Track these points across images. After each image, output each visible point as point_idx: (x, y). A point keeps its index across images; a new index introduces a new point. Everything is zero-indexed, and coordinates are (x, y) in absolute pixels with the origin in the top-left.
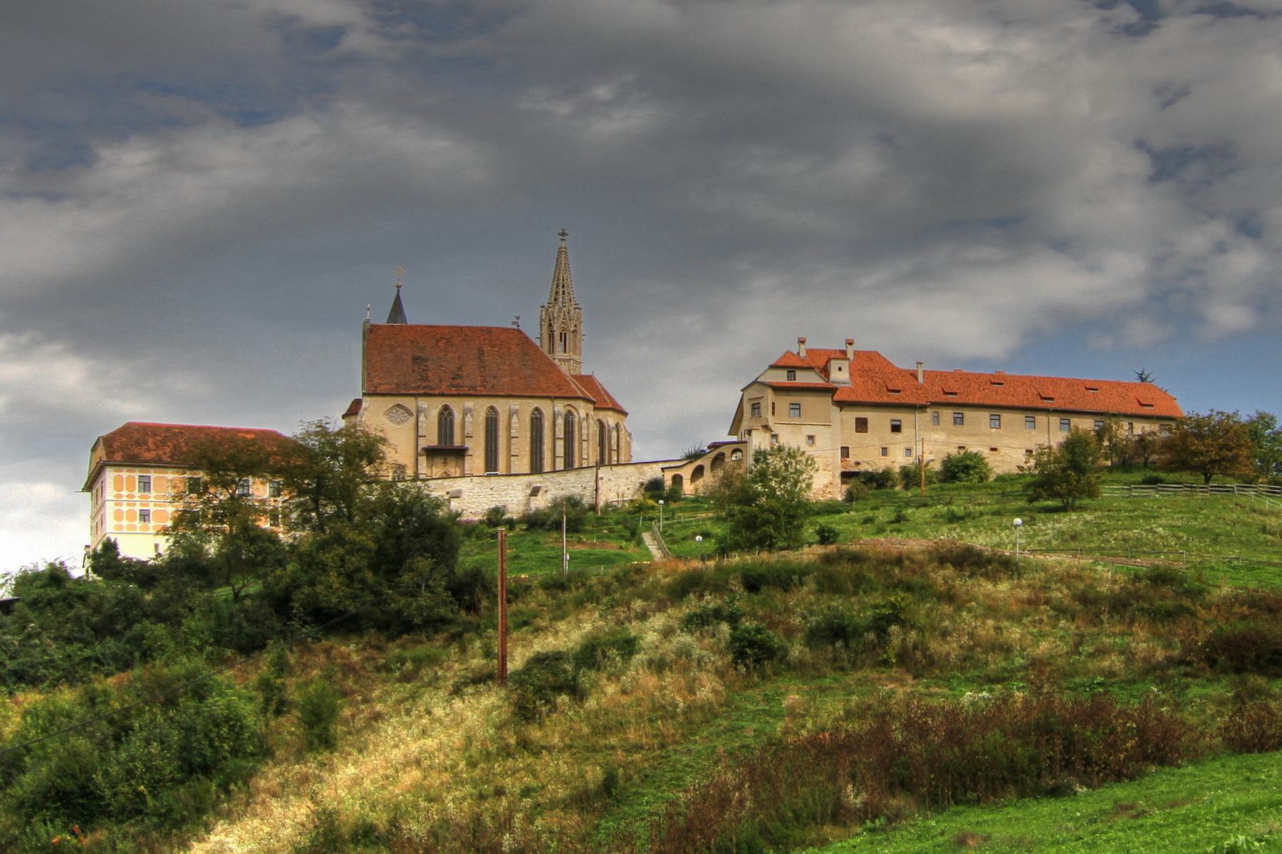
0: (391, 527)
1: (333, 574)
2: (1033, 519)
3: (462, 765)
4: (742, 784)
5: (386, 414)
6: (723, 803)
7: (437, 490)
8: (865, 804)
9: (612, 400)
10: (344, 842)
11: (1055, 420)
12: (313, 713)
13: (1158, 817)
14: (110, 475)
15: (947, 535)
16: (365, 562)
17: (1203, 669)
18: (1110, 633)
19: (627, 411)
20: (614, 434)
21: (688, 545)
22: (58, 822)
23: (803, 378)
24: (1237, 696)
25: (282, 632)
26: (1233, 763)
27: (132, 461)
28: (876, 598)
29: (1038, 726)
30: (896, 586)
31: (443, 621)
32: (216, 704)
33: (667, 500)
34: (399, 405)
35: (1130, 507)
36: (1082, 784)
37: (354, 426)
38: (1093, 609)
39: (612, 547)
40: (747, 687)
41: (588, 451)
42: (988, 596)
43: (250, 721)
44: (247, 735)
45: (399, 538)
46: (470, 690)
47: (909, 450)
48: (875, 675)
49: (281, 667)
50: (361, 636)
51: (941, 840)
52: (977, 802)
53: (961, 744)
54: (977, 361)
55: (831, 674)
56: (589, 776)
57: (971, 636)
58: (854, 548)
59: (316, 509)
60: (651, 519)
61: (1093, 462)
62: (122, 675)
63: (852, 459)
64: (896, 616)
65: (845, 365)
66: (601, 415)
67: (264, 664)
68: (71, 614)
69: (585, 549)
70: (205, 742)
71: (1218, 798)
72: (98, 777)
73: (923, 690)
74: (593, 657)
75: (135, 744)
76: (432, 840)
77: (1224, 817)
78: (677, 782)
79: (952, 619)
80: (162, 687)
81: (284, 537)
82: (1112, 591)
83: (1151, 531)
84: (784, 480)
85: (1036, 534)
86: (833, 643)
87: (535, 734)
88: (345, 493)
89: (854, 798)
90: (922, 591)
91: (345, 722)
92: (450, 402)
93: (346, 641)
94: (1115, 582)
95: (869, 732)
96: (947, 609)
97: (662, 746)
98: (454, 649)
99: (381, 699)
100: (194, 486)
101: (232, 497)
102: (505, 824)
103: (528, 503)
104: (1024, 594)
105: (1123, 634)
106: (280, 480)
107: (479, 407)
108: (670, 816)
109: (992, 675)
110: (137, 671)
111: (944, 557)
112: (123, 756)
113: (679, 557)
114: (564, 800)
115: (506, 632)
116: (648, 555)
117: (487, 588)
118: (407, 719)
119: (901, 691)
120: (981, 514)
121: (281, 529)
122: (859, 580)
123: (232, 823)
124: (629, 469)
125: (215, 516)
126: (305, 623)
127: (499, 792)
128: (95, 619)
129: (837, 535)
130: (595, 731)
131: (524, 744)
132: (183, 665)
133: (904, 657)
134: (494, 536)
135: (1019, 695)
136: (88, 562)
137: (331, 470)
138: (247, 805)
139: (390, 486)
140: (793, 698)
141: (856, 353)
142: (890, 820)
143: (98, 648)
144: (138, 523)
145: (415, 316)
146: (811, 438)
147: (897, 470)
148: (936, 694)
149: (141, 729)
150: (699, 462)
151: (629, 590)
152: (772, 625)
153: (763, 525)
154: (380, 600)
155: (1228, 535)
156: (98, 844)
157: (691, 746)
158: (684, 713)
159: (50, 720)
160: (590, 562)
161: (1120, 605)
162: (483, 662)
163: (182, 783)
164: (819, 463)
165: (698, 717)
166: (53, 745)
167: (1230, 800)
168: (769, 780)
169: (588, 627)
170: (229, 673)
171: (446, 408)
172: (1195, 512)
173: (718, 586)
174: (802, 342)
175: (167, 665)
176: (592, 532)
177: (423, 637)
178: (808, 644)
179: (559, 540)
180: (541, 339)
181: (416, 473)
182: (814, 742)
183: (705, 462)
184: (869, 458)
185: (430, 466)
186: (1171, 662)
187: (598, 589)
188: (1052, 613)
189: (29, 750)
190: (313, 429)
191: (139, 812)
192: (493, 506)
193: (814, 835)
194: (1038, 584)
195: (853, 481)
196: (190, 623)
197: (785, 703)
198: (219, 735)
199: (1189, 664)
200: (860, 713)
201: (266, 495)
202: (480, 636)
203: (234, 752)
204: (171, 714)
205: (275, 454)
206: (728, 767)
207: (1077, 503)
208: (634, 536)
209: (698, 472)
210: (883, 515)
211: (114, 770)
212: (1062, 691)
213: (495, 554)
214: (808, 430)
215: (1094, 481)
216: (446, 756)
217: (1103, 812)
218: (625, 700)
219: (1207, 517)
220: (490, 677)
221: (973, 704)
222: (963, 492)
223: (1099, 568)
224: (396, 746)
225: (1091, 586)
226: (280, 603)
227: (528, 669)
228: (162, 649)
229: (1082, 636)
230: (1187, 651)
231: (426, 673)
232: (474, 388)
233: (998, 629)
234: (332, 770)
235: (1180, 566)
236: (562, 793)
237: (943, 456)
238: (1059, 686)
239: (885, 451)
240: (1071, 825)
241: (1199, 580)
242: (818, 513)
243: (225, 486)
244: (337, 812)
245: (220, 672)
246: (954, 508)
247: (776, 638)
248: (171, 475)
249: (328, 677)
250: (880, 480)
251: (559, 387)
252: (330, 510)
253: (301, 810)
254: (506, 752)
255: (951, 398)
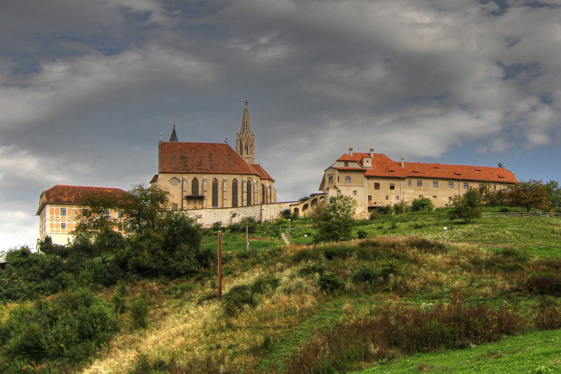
0: (171, 231)
1: (146, 251)
2: (452, 227)
3: (202, 335)
4: (325, 343)
5: (169, 181)
6: (317, 352)
7: (191, 215)
8: (379, 352)
9: (268, 175)
10: (151, 369)
11: (462, 184)
12: (137, 312)
13: (507, 358)
14: (48, 208)
15: (414, 234)
16: (160, 246)
17: (527, 293)
18: (486, 277)
19: (274, 180)
20: (269, 190)
21: (301, 239)
22: (26, 360)
23: (351, 166)
24: (541, 305)
25: (123, 277)
26: (540, 334)
27: (58, 202)
28: (383, 262)
29: (454, 318)
30: (392, 257)
31: (194, 272)
32: (95, 308)
33: (292, 219)
34: (174, 178)
35: (495, 222)
36: (474, 343)
37: (155, 187)
38: (478, 267)
39: (268, 240)
40: (327, 301)
41: (257, 197)
42: (432, 261)
43: (109, 316)
44: (108, 322)
45: (175, 235)
46: (206, 302)
47: (398, 197)
48: (383, 296)
49: (123, 292)
50: (158, 279)
51: (412, 368)
52: (428, 351)
53: (420, 326)
54: (428, 158)
55: (363, 295)
56: (258, 340)
57: (425, 278)
58: (374, 240)
59: (138, 223)
60: (285, 227)
61: (478, 202)
62: (54, 295)
63: (373, 201)
64: (392, 270)
66: (263, 182)
67: (115, 291)
68: (31, 269)
69: (256, 240)
70: (90, 325)
71: (533, 350)
72: (43, 340)
73: (404, 302)
74: (259, 288)
75: (59, 326)
76: (189, 368)
77: (536, 358)
78: (296, 343)
79: (417, 271)
80: (71, 301)
81: (124, 235)
82: (487, 259)
83: (504, 232)
84: (343, 210)
85: (453, 234)
86: (364, 282)
87: (234, 321)
88: (151, 216)
89: (374, 349)
90: (404, 259)
91: (151, 316)
92: (197, 176)
93: (151, 281)
94: (488, 255)
95: (380, 321)
96: (414, 267)
97: (290, 327)
98: (199, 284)
99: (167, 306)
100: (85, 213)
101: (102, 218)
102: (221, 361)
103: (231, 220)
104: (448, 260)
105: (491, 278)
106: (123, 210)
107: (210, 178)
108: (293, 357)
109: (434, 296)
110: (60, 294)
111: (413, 244)
112: (54, 331)
113: (297, 244)
114: (247, 351)
115: (221, 277)
116: (284, 243)
117: (213, 258)
118: (178, 315)
119: (394, 302)
120: (429, 225)
121: (123, 231)
122: (376, 254)
123: (102, 360)
124: (275, 205)
125: (94, 226)
126: (133, 273)
127: (219, 347)
128: (41, 271)
129: (366, 234)
130: (260, 320)
131: (230, 326)
132: (80, 291)
133: (396, 288)
134: (216, 235)
135: (446, 304)
136: (39, 246)
137: (145, 206)
138: (108, 352)
139: (171, 213)
140: (347, 306)
141: (375, 155)
142: (389, 359)
143: (43, 284)
144: (60, 229)
145: (182, 138)
146: (355, 192)
147: (393, 206)
148: (410, 304)
149: (62, 319)
150: (306, 202)
151: (275, 259)
152: (338, 274)
153: (334, 230)
154: (166, 263)
155: (537, 234)
156: (43, 369)
157: (302, 327)
158: (300, 312)
159: (22, 316)
160: (258, 246)
161: (490, 265)
162: (211, 290)
163: (80, 343)
164: (359, 203)
165: (305, 314)
166: (23, 326)
167: (538, 351)
168: (336, 342)
169: (257, 275)
170: (100, 295)
171: (195, 179)
172: (523, 224)
173: (314, 257)
174: (351, 150)
175: (73, 291)
176: (259, 233)
177: (185, 279)
178: (354, 282)
179: (245, 237)
180: (237, 148)
181: (182, 207)
182: (356, 325)
183: (309, 202)
184: (380, 201)
185: (188, 204)
186: (512, 290)
187: (262, 258)
188: (460, 268)
189: (12, 329)
190: (137, 188)
191: (61, 356)
192: (216, 221)
193: (356, 366)
194: (454, 256)
195: (373, 211)
196: (83, 273)
197: (344, 308)
198: (96, 322)
199: (520, 291)
200: (376, 312)
201: (117, 217)
202: (210, 279)
203: (103, 329)
204: (75, 312)
205: (120, 199)
206: (318, 336)
207: (472, 220)
208: (277, 235)
209: (306, 207)
210: (386, 226)
211: (50, 337)
212: (465, 303)
213: (216, 243)
214: (354, 189)
215: (479, 210)
216: (195, 331)
217: (483, 356)
218: (273, 306)
219: (528, 227)
220: (214, 296)
221: (426, 308)
222: (421, 216)
223: (481, 249)
224: (173, 327)
225: (477, 257)
226: (123, 264)
227: (231, 293)
228: (71, 284)
229: (474, 278)
230: (519, 285)
231: (187, 295)
232: (207, 170)
233: (437, 275)
234: (145, 337)
235: (516, 248)
236: (246, 347)
237: (413, 200)
238: (463, 300)
239: (387, 198)
240: (468, 361)
241: (525, 254)
242: (358, 225)
243: (99, 213)
244: (148, 356)
245: (96, 294)
246: (417, 222)
247: (339, 279)
248: (75, 208)
249: (144, 297)
250: (385, 210)
251: (245, 170)
252: (144, 223)
253: (132, 355)
254: (221, 329)
255: (416, 174)
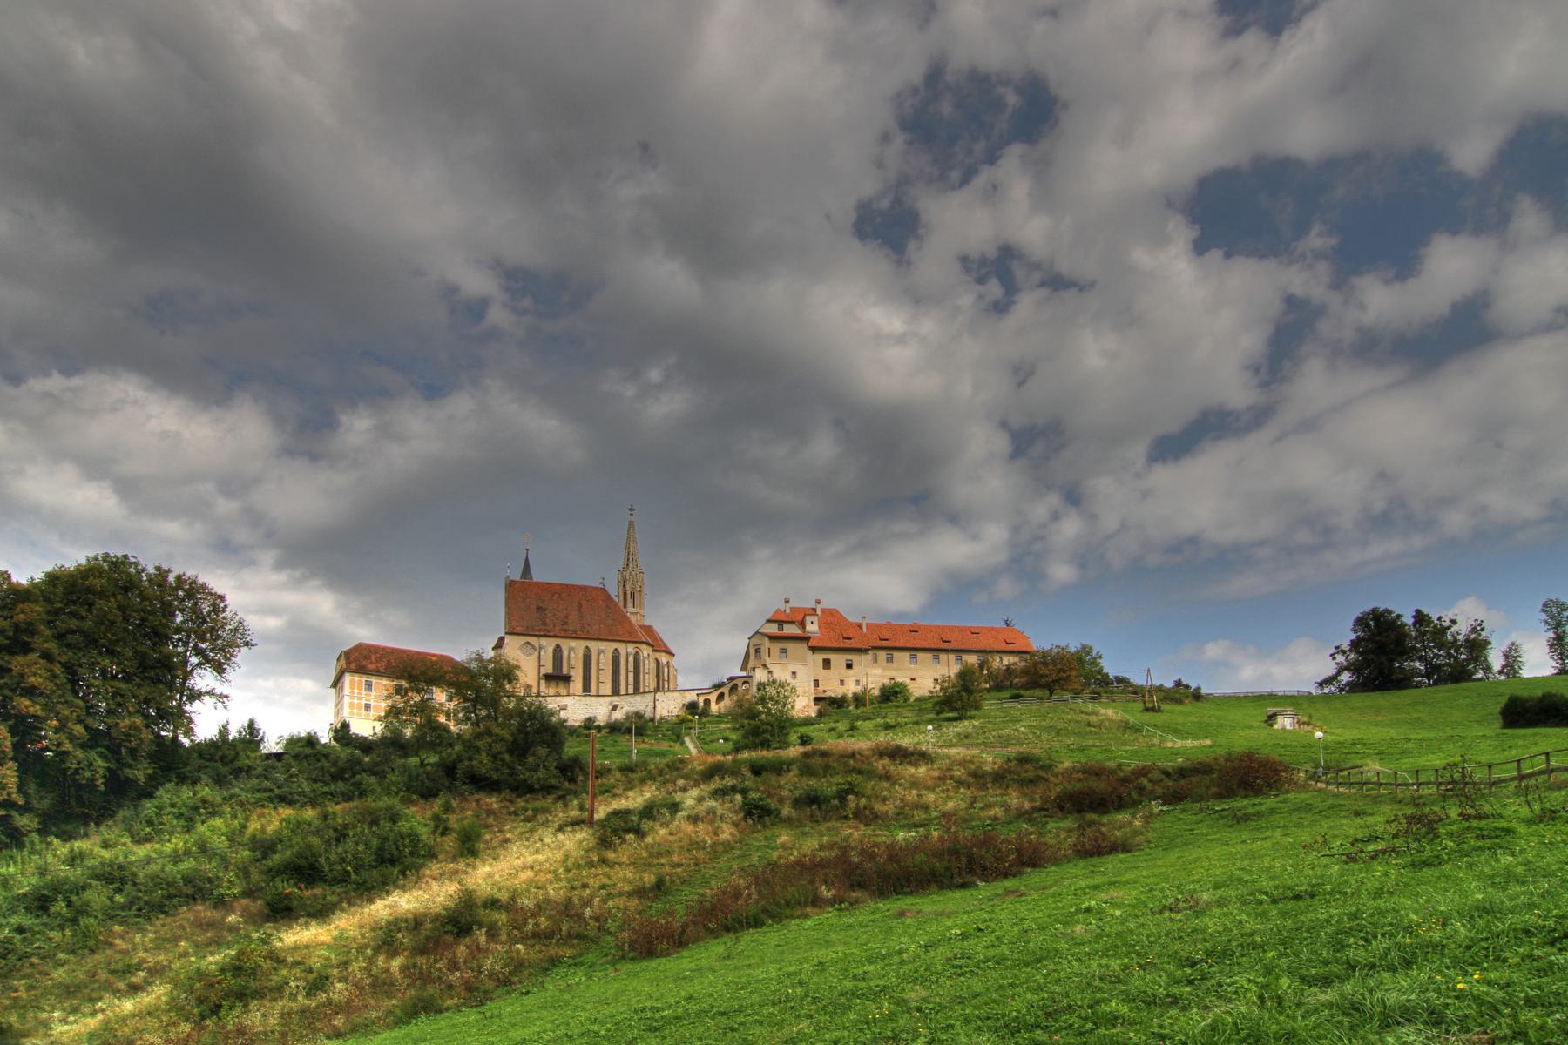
0: (522, 726)
1: (484, 754)
2: (940, 726)
3: (561, 870)
4: (750, 886)
7: (552, 704)
9: (664, 644)
11: (952, 657)
12: (465, 835)
13: (1035, 895)
14: (348, 678)
15: (884, 738)
16: (504, 748)
18: (994, 795)
19: (674, 652)
20: (666, 669)
21: (714, 746)
22: (292, 882)
24: (1080, 827)
25: (449, 787)
26: (1081, 863)
27: (361, 670)
28: (839, 779)
29: (949, 850)
30: (851, 771)
32: (404, 826)
33: (700, 715)
34: (528, 643)
35: (1002, 715)
36: (981, 880)
37: (500, 656)
38: (981, 781)
40: (753, 832)
41: (649, 681)
42: (912, 776)
43: (424, 837)
45: (527, 734)
46: (569, 829)
47: (858, 681)
48: (839, 825)
49: (447, 808)
51: (888, 913)
52: (911, 893)
56: (646, 880)
58: (823, 747)
59: (475, 712)
60: (690, 728)
61: (978, 685)
63: (821, 688)
64: (853, 789)
65: (815, 619)
66: (657, 655)
67: (437, 805)
68: (318, 765)
69: (647, 746)
71: (1075, 883)
72: (322, 860)
75: (349, 844)
76: (537, 909)
77: (1080, 892)
78: (706, 884)
79: (889, 790)
80: (370, 813)
81: (454, 729)
82: (993, 769)
83: (1017, 730)
84: (777, 703)
85: (942, 736)
86: (810, 807)
87: (611, 855)
88: (493, 702)
89: (826, 892)
90: (869, 774)
91: (486, 842)
94: (995, 763)
96: (886, 784)
97: (696, 865)
98: (560, 805)
99: (510, 831)
101: (422, 700)
103: (610, 716)
104: (936, 774)
105: (1002, 795)
107: (579, 646)
110: (355, 803)
111: (882, 753)
113: (708, 753)
114: (628, 892)
115: (594, 796)
116: (689, 752)
117: (583, 769)
118: (526, 843)
119: (856, 833)
120: (906, 724)
121: (452, 723)
122: (827, 769)
123: (405, 891)
125: (411, 711)
126: (464, 783)
127: (585, 886)
128: (332, 770)
129: (812, 739)
130: (651, 855)
131: (603, 861)
132: (385, 802)
133: (858, 815)
134: (588, 736)
135: (935, 834)
136: (331, 734)
138: (416, 883)
140: (784, 838)
141: (823, 610)
142: (851, 904)
143: (333, 787)
144: (363, 712)
145: (539, 575)
146: (794, 673)
147: (850, 695)
148: (880, 835)
149: (354, 836)
150: (721, 690)
151: (676, 773)
152: (770, 796)
153: (764, 733)
154: (513, 772)
155: (1066, 729)
156: (315, 896)
158: (711, 846)
159: (297, 826)
160: (650, 755)
161: (999, 778)
162: (578, 813)
163: (376, 868)
164: (800, 691)
165: (720, 848)
166: (296, 840)
167: (1082, 883)
168: (768, 883)
169: (648, 795)
172: (1044, 716)
173: (734, 771)
174: (787, 602)
175: (374, 801)
176: (651, 736)
177: (540, 796)
178: (794, 807)
180: (618, 596)
181: (539, 691)
183: (725, 690)
184: (833, 689)
185: (548, 687)
186: (1034, 809)
187: (655, 772)
188: (954, 784)
189: (281, 841)
190: (474, 656)
191: (346, 881)
192: (587, 716)
194: (945, 767)
195: (822, 703)
196: (392, 777)
197: (778, 842)
198: (403, 844)
199: (1047, 810)
200: (831, 846)
201: (443, 701)
202: (577, 799)
203: (412, 854)
204: (374, 829)
205: (450, 672)
209: (721, 697)
211: (333, 857)
212: (963, 830)
213: (588, 748)
215: (978, 699)
216: (551, 865)
218: (671, 838)
219: (1052, 719)
220: (583, 822)
221: (905, 839)
222: (894, 709)
223: (984, 755)
224: (518, 858)
225: (979, 767)
226: (449, 770)
228: (373, 791)
229: (975, 797)
230: (1045, 801)
232: (576, 632)
233: (919, 796)
234: (474, 868)
235: (1036, 751)
236: (627, 888)
237: (880, 685)
238: (962, 827)
239: (842, 682)
240: (975, 902)
242: (799, 725)
243: (418, 692)
244: (475, 891)
245: (408, 808)
246: (889, 720)
247: (772, 803)
248: (385, 682)
250: (838, 703)
251: (630, 634)
252: (483, 713)
253: (451, 888)
254: (591, 865)
255: (885, 644)
